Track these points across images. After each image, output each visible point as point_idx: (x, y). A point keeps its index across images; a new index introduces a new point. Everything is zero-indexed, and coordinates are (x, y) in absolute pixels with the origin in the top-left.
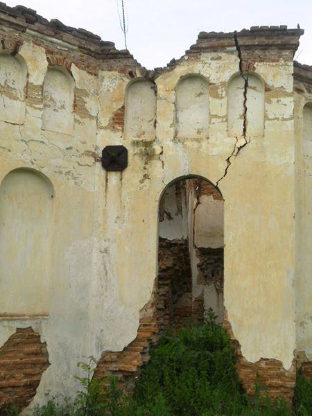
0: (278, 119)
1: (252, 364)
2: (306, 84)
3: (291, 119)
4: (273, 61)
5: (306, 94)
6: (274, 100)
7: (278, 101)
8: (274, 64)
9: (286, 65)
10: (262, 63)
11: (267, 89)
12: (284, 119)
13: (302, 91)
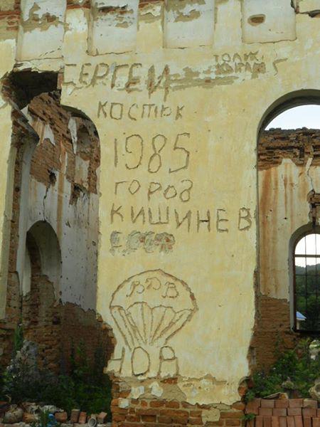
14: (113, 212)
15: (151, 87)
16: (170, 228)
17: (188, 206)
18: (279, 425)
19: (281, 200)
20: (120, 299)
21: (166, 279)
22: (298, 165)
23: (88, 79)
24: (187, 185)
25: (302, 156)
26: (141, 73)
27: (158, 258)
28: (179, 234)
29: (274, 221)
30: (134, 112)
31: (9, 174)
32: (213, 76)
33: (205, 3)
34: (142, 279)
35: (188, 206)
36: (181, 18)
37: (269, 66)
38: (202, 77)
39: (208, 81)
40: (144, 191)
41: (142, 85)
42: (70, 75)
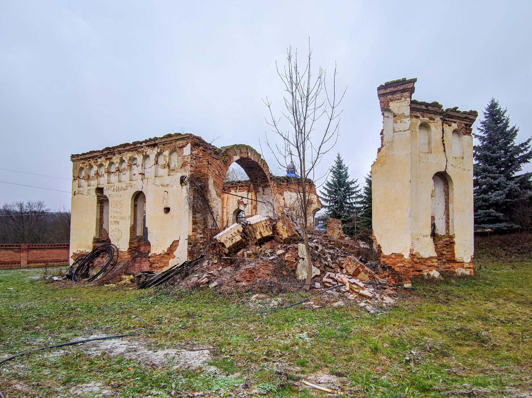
0: (401, 131)
1: (387, 256)
2: (421, 113)
3: (408, 130)
4: (398, 100)
5: (421, 118)
6: (399, 121)
7: (401, 121)
8: (398, 101)
9: (406, 100)
10: (392, 102)
11: (395, 116)
12: (404, 131)
13: (419, 117)
14: (111, 217)
15: (117, 191)
16: (119, 220)
17: (121, 215)
18: (2, 246)
19: (231, 203)
20: (112, 234)
21: (118, 230)
22: (235, 192)
23: (107, 189)
24: (121, 211)
25: (236, 189)
26: (115, 187)
27: (117, 226)
28: (120, 221)
29: (229, 208)
30: (114, 196)
31: (97, 209)
32: (125, 188)
33: (417, 78)
34: (115, 230)
35: (121, 215)
36: (124, 174)
37: (133, 186)
38: (124, 188)
39: (125, 189)
40: (115, 213)
41: (115, 190)
42: (105, 189)
